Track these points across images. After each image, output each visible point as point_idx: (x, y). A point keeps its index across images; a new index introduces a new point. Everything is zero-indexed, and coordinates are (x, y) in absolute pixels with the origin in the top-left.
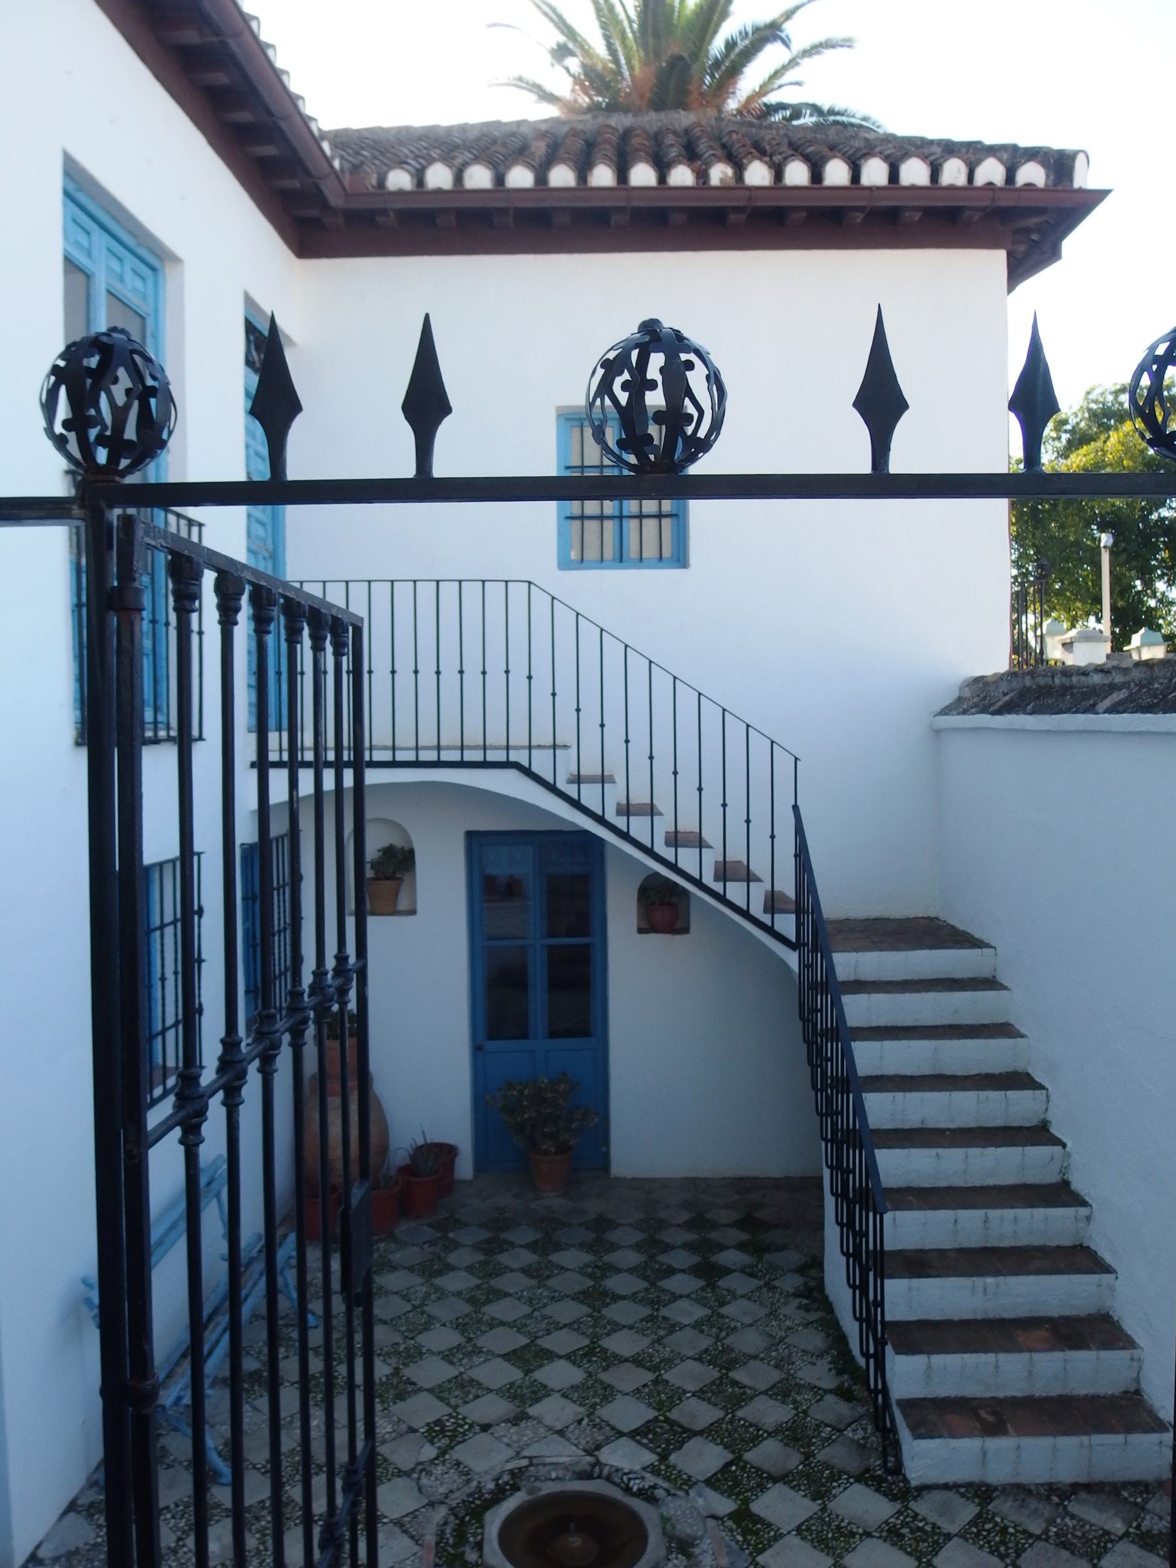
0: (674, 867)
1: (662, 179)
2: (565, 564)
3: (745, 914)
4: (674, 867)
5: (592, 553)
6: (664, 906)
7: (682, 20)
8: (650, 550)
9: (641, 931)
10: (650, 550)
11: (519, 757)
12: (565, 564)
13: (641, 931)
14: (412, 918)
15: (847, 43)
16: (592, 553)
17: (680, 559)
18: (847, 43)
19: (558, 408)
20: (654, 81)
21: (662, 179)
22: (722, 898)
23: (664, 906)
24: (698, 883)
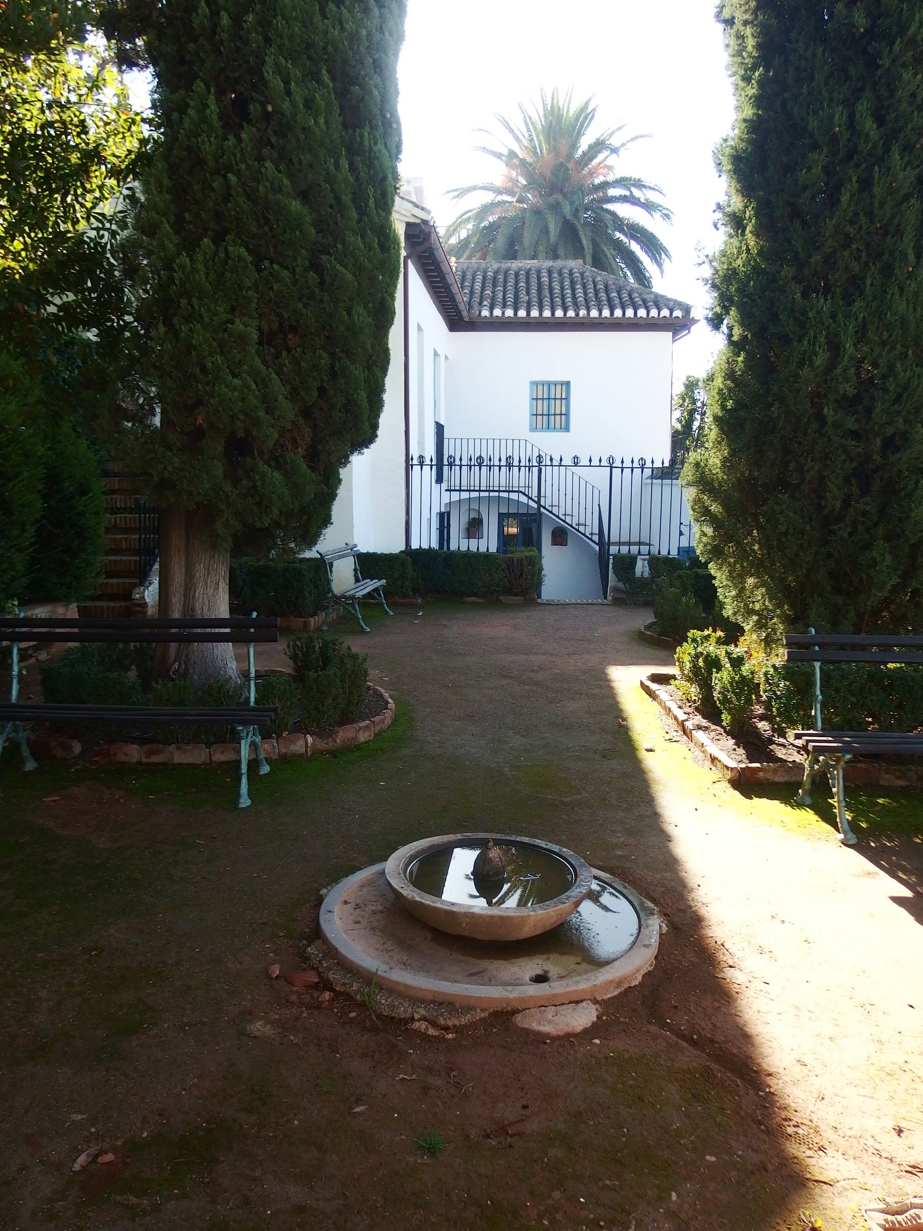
0: (564, 521)
1: (565, 314)
2: (531, 430)
3: (584, 535)
4: (564, 521)
5: (539, 426)
6: (560, 536)
7: (568, 122)
8: (558, 426)
9: (568, 431)
10: (558, 426)
11: (522, 489)
12: (531, 430)
13: (568, 431)
14: (571, 384)
15: (650, 136)
16: (539, 426)
17: (567, 429)
18: (650, 136)
19: (688, 377)
20: (548, 174)
21: (565, 314)
22: (578, 530)
23: (560, 536)
24: (571, 526)
